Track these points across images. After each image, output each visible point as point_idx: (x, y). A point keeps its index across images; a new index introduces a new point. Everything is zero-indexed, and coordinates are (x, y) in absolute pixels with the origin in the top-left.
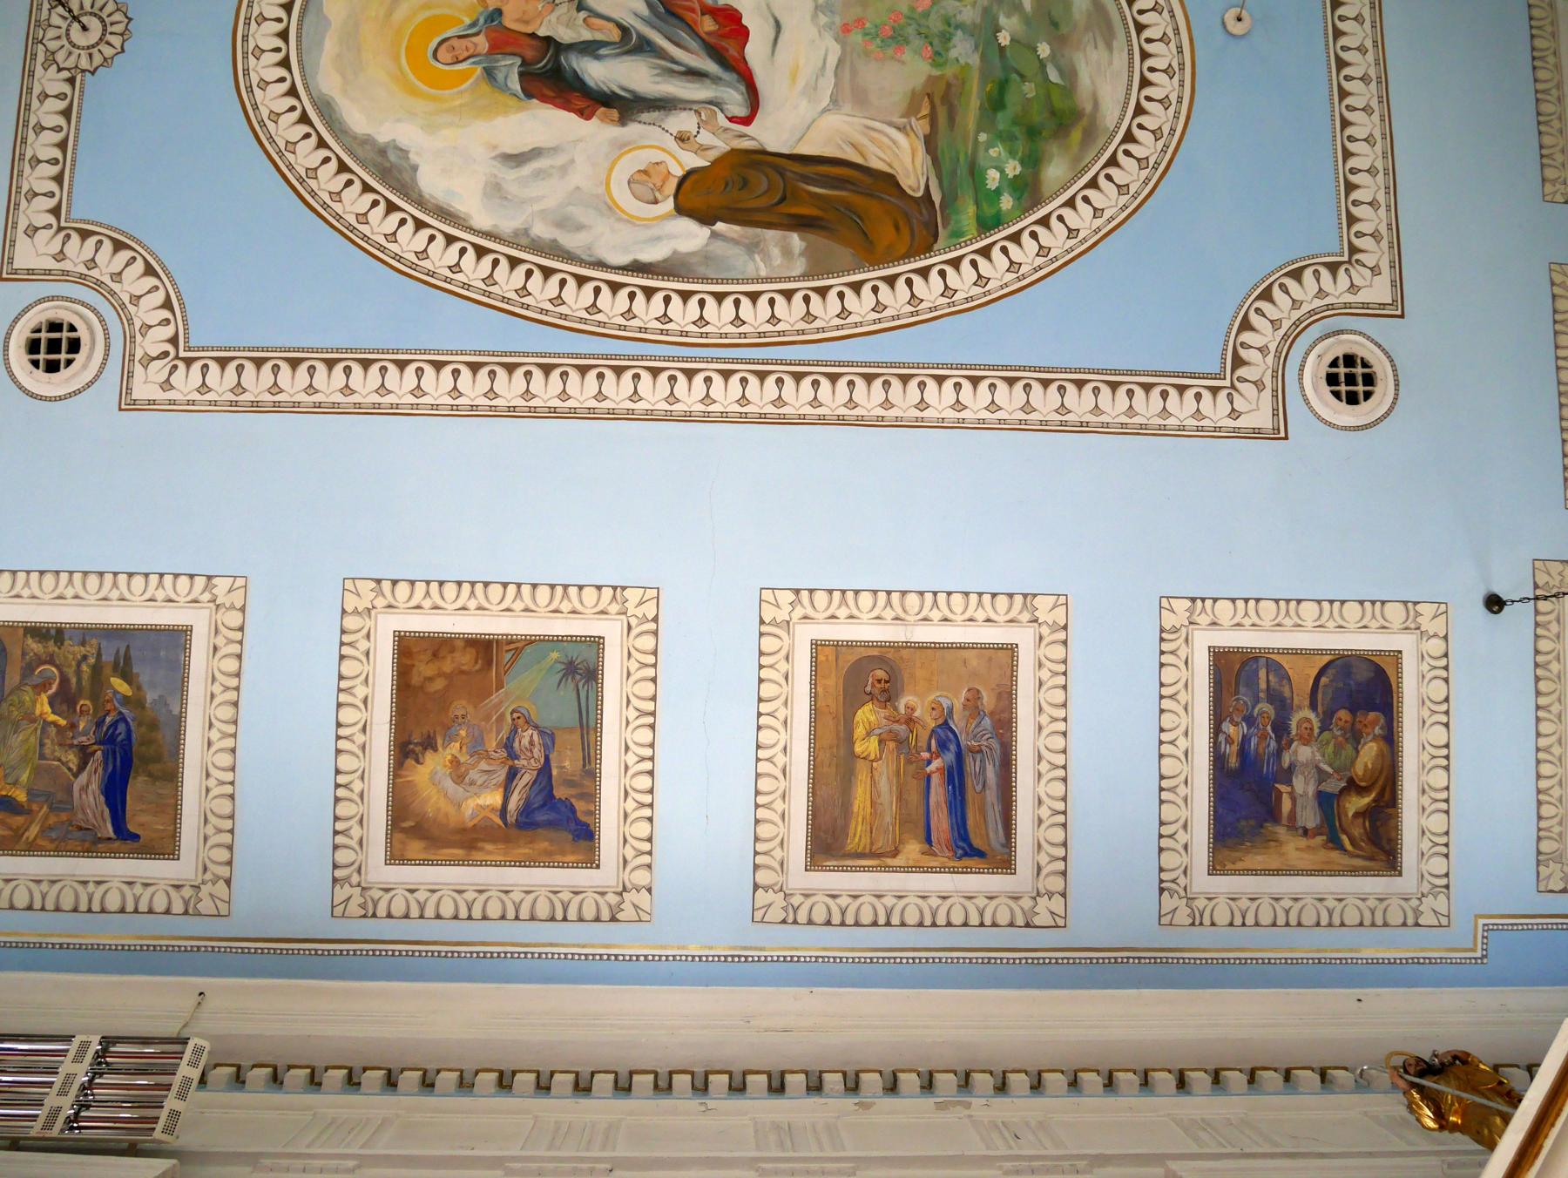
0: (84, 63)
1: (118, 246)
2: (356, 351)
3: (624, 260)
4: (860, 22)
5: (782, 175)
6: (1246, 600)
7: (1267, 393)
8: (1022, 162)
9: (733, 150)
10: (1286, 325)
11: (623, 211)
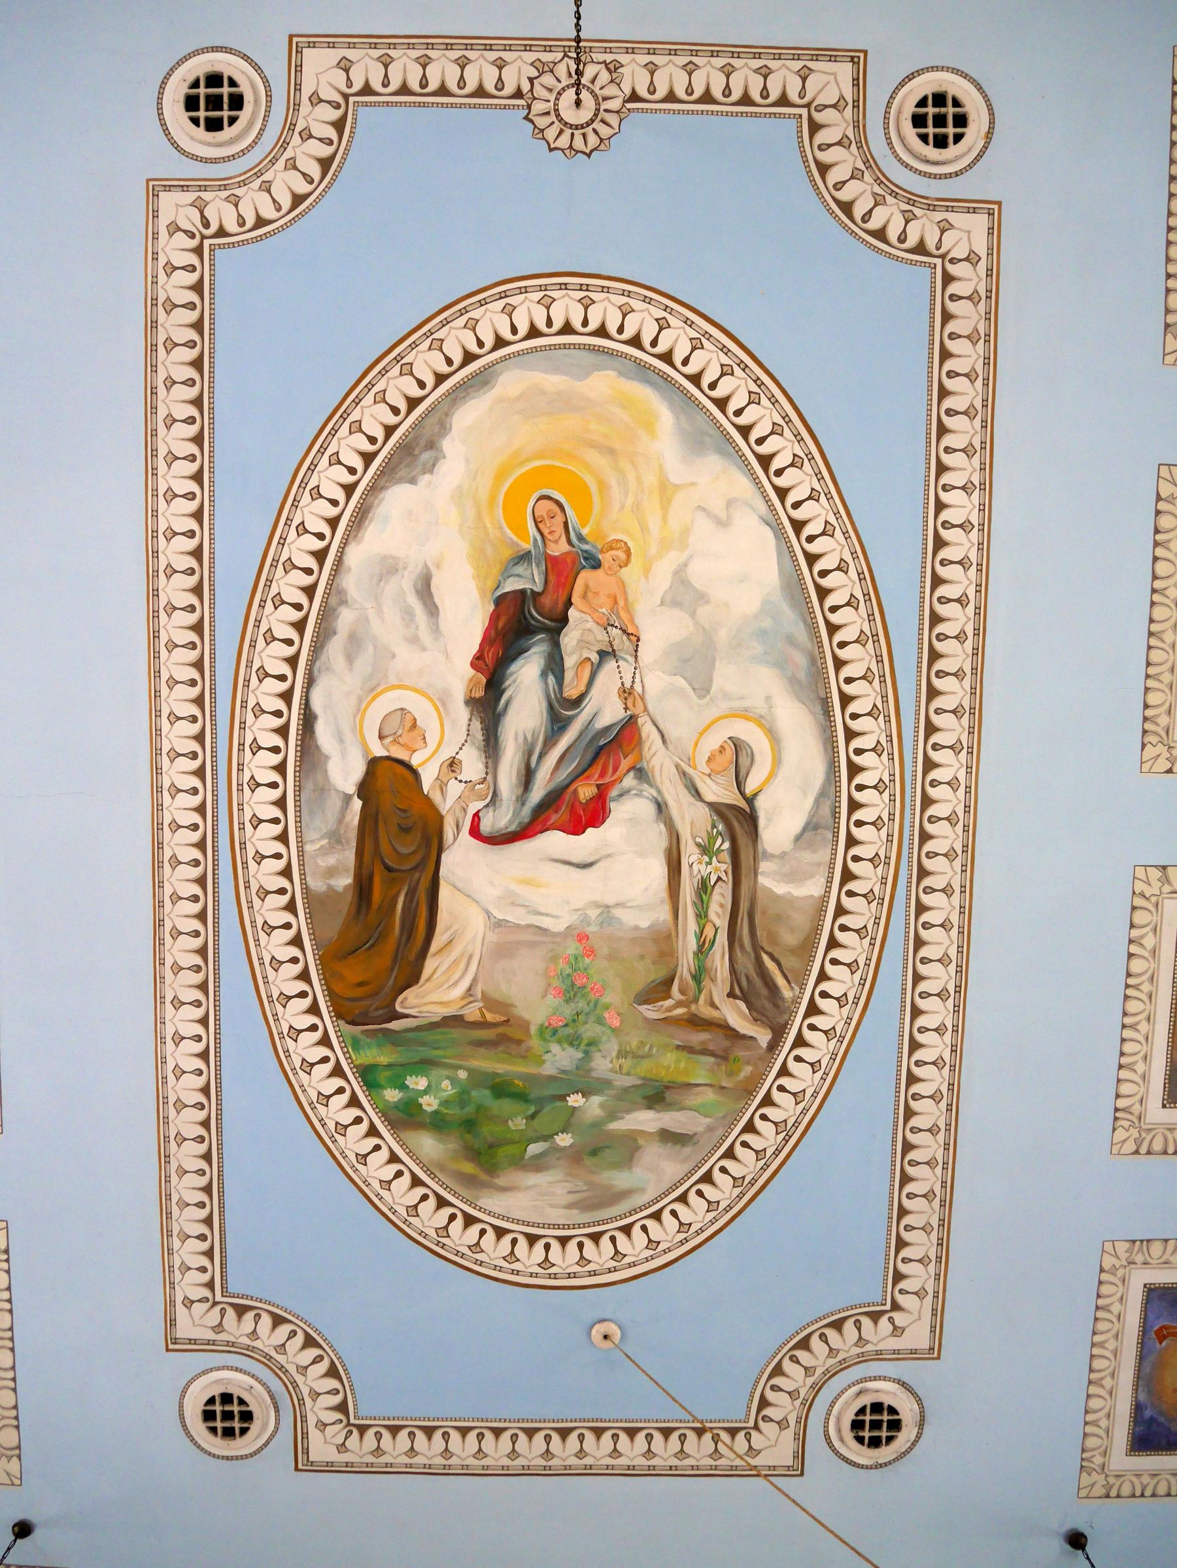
0: (538, 107)
1: (325, 164)
2: (212, 429)
3: (317, 705)
4: (591, 952)
5: (415, 868)
6: (10, 1301)
7: (211, 1336)
8: (436, 1112)
9: (442, 817)
10: (281, 1358)
11: (370, 703)
